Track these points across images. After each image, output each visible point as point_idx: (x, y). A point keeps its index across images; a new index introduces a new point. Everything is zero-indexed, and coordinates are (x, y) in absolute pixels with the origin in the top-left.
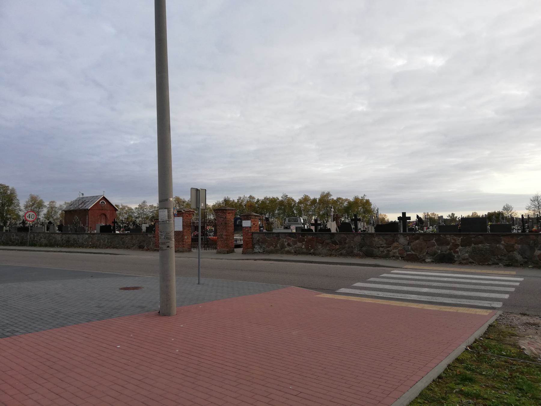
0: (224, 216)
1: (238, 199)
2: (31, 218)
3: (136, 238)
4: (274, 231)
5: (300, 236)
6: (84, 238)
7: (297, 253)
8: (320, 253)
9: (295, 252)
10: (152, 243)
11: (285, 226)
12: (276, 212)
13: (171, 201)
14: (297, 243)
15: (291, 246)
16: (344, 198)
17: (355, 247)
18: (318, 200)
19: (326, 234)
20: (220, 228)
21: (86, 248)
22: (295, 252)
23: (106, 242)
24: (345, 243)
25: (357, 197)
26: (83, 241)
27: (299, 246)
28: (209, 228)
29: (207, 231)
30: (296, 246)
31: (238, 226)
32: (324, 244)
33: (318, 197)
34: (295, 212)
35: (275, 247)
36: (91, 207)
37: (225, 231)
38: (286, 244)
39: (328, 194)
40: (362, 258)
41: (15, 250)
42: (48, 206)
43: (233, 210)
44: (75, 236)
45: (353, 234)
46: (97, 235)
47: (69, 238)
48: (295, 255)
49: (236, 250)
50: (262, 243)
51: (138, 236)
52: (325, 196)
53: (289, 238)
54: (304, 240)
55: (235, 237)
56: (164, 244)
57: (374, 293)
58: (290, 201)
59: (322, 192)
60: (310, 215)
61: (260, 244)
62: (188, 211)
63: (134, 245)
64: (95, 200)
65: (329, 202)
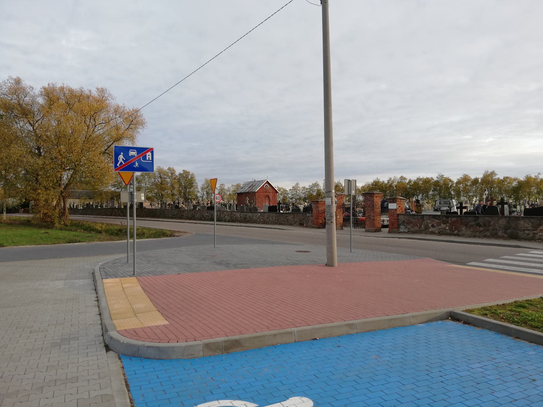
0: (372, 199)
1: (388, 180)
2: (217, 199)
3: (297, 217)
4: (423, 213)
5: (444, 218)
6: (257, 216)
7: (440, 233)
8: (464, 235)
9: (439, 233)
10: (310, 221)
11: (435, 208)
12: (431, 193)
13: (333, 192)
14: (441, 225)
15: (435, 227)
16: (513, 177)
17: (499, 230)
18: (480, 180)
19: (471, 216)
20: (369, 210)
21: (258, 224)
22: (439, 233)
23: (274, 219)
24: (490, 226)
25: (529, 176)
26: (257, 219)
27: (443, 228)
28: (358, 210)
29: (356, 212)
30: (440, 227)
31: (385, 207)
32: (468, 226)
33: (480, 176)
34: (452, 193)
35: (419, 228)
36: (258, 190)
37: (373, 212)
38: (430, 225)
39: (493, 173)
40: (506, 240)
41: (208, 224)
42: (219, 188)
43: (380, 194)
44: (250, 214)
45: (498, 217)
46: (267, 214)
47: (245, 215)
48: (438, 235)
49: (382, 229)
50: (407, 223)
51: (299, 215)
52: (489, 175)
53: (433, 220)
54: (448, 221)
55: (382, 218)
56: (329, 220)
57: (494, 266)
58: (447, 182)
59: (485, 171)
60: (470, 196)
61: (405, 224)
62: (340, 195)
63: (296, 222)
64: (261, 184)
65: (494, 181)
